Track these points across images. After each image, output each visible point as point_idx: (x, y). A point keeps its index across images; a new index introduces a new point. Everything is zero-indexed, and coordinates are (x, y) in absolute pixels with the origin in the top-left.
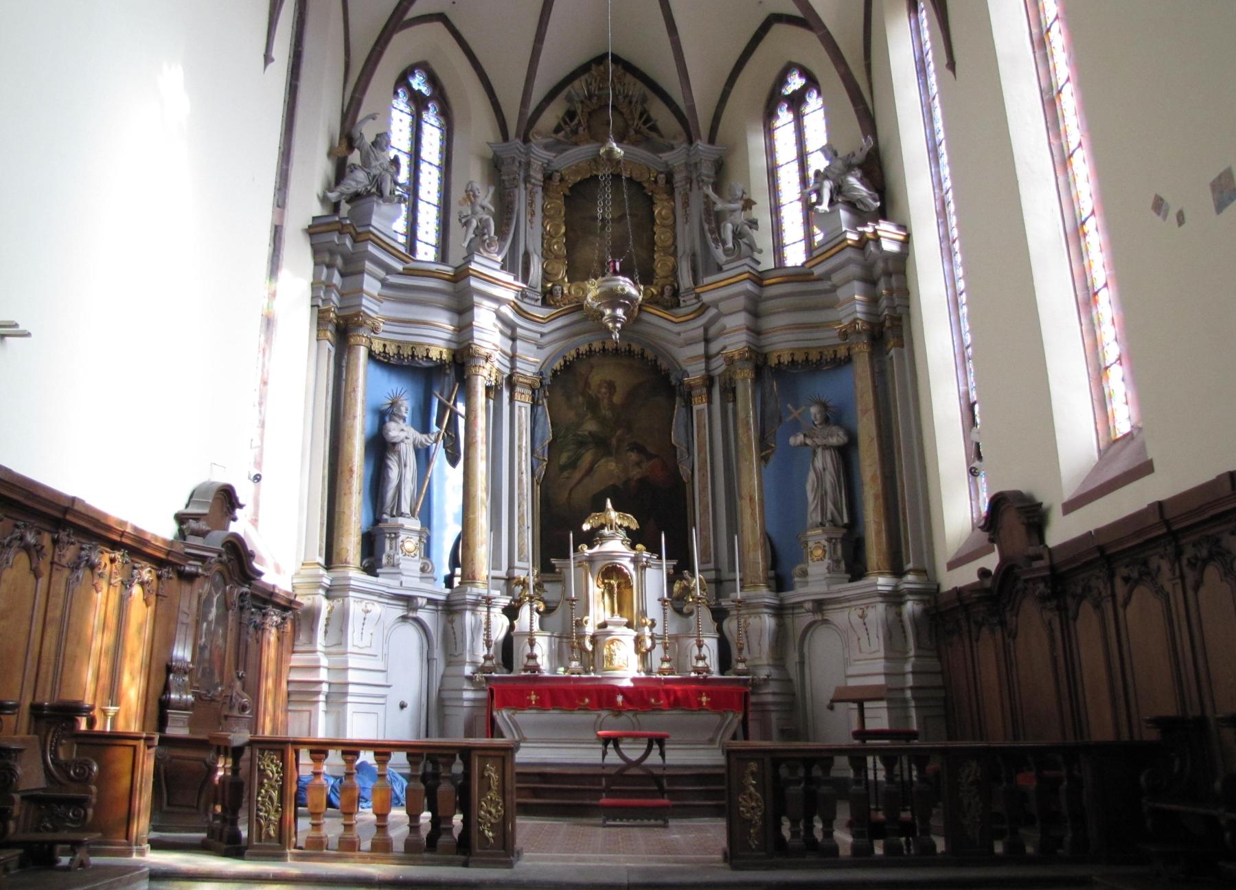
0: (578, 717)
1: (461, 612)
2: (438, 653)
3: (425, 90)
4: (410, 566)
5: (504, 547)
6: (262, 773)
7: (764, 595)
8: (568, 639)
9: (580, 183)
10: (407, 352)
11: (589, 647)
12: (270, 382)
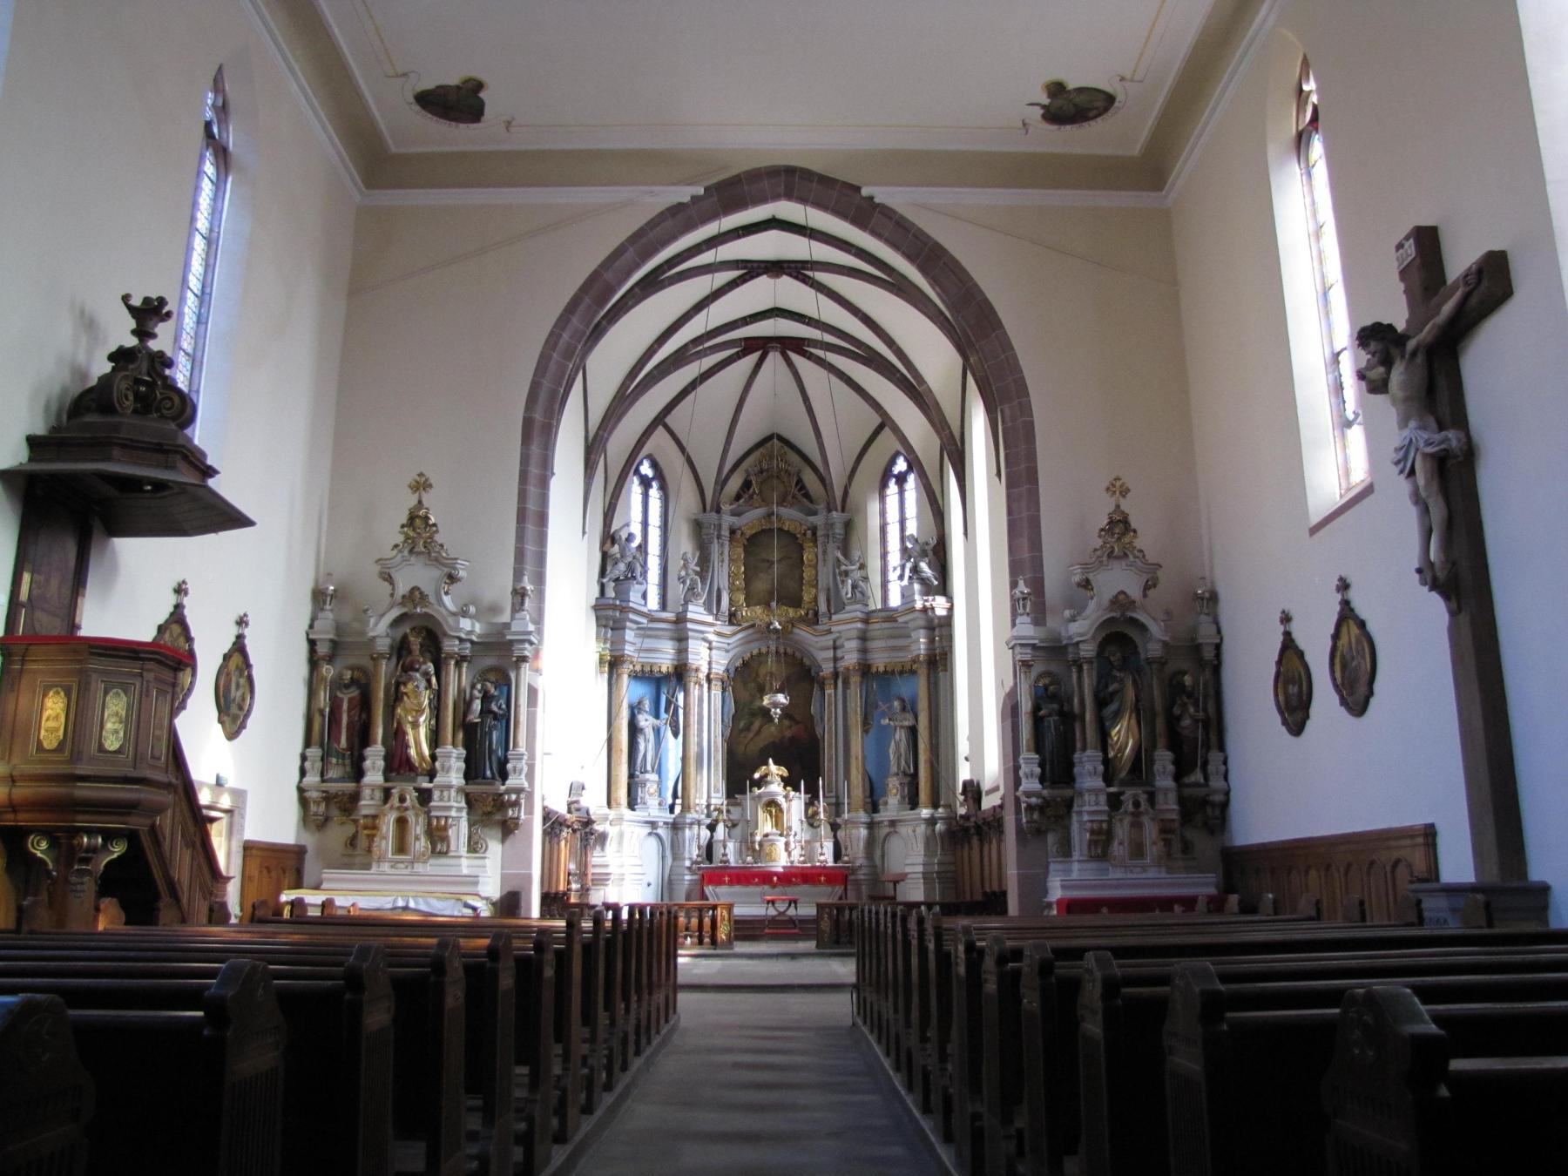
0: (751, 889)
1: (683, 829)
2: (668, 853)
4: (653, 802)
5: (709, 789)
7: (863, 816)
8: (747, 844)
10: (647, 669)
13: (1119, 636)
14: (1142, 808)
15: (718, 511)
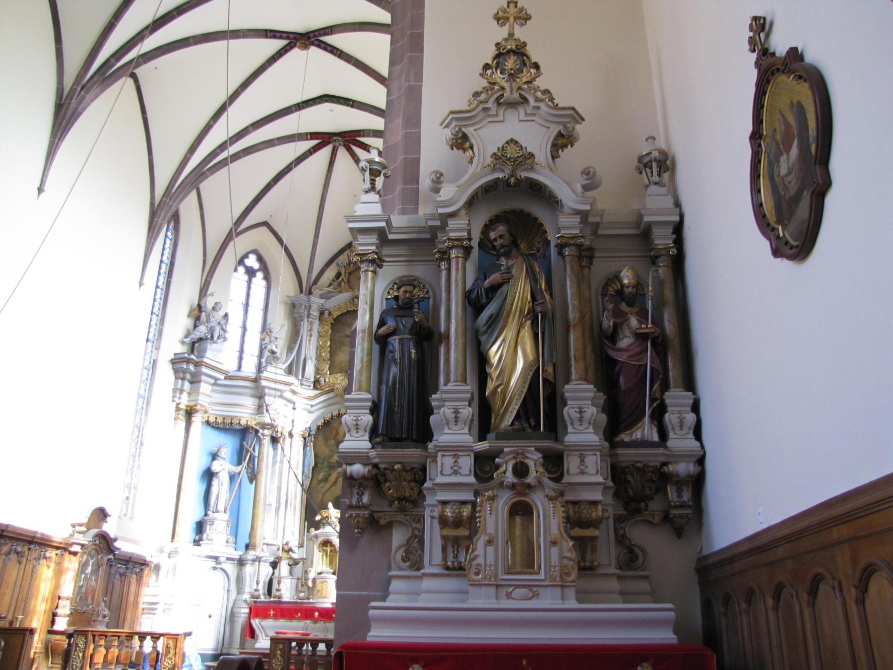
2: (233, 587)
3: (256, 266)
6: (77, 645)
8: (302, 582)
9: (341, 315)
10: (228, 421)
11: (310, 584)
12: (144, 444)
13: (513, 210)
14: (531, 479)
15: (310, 293)
